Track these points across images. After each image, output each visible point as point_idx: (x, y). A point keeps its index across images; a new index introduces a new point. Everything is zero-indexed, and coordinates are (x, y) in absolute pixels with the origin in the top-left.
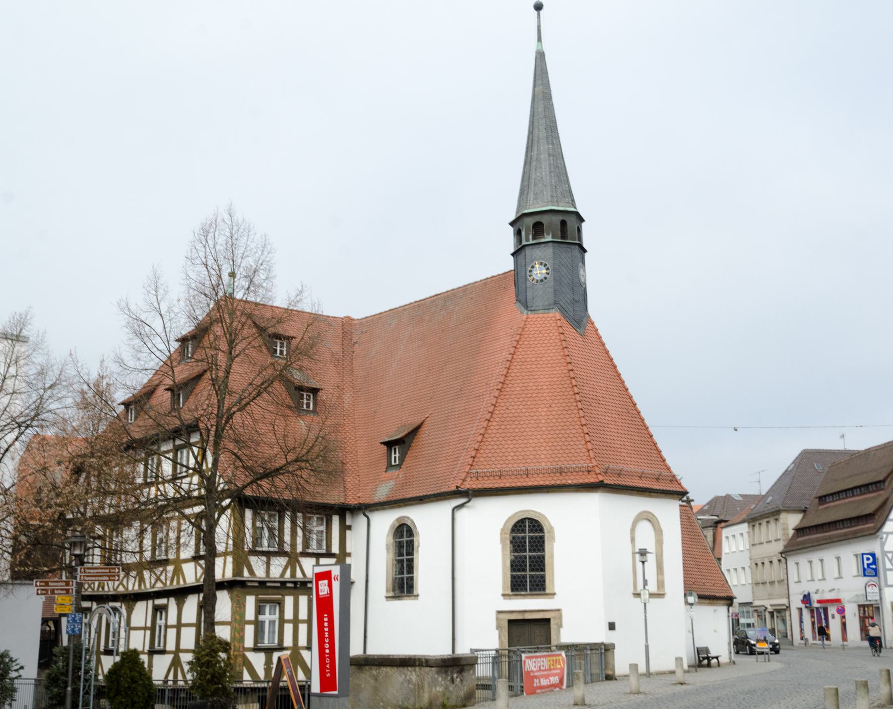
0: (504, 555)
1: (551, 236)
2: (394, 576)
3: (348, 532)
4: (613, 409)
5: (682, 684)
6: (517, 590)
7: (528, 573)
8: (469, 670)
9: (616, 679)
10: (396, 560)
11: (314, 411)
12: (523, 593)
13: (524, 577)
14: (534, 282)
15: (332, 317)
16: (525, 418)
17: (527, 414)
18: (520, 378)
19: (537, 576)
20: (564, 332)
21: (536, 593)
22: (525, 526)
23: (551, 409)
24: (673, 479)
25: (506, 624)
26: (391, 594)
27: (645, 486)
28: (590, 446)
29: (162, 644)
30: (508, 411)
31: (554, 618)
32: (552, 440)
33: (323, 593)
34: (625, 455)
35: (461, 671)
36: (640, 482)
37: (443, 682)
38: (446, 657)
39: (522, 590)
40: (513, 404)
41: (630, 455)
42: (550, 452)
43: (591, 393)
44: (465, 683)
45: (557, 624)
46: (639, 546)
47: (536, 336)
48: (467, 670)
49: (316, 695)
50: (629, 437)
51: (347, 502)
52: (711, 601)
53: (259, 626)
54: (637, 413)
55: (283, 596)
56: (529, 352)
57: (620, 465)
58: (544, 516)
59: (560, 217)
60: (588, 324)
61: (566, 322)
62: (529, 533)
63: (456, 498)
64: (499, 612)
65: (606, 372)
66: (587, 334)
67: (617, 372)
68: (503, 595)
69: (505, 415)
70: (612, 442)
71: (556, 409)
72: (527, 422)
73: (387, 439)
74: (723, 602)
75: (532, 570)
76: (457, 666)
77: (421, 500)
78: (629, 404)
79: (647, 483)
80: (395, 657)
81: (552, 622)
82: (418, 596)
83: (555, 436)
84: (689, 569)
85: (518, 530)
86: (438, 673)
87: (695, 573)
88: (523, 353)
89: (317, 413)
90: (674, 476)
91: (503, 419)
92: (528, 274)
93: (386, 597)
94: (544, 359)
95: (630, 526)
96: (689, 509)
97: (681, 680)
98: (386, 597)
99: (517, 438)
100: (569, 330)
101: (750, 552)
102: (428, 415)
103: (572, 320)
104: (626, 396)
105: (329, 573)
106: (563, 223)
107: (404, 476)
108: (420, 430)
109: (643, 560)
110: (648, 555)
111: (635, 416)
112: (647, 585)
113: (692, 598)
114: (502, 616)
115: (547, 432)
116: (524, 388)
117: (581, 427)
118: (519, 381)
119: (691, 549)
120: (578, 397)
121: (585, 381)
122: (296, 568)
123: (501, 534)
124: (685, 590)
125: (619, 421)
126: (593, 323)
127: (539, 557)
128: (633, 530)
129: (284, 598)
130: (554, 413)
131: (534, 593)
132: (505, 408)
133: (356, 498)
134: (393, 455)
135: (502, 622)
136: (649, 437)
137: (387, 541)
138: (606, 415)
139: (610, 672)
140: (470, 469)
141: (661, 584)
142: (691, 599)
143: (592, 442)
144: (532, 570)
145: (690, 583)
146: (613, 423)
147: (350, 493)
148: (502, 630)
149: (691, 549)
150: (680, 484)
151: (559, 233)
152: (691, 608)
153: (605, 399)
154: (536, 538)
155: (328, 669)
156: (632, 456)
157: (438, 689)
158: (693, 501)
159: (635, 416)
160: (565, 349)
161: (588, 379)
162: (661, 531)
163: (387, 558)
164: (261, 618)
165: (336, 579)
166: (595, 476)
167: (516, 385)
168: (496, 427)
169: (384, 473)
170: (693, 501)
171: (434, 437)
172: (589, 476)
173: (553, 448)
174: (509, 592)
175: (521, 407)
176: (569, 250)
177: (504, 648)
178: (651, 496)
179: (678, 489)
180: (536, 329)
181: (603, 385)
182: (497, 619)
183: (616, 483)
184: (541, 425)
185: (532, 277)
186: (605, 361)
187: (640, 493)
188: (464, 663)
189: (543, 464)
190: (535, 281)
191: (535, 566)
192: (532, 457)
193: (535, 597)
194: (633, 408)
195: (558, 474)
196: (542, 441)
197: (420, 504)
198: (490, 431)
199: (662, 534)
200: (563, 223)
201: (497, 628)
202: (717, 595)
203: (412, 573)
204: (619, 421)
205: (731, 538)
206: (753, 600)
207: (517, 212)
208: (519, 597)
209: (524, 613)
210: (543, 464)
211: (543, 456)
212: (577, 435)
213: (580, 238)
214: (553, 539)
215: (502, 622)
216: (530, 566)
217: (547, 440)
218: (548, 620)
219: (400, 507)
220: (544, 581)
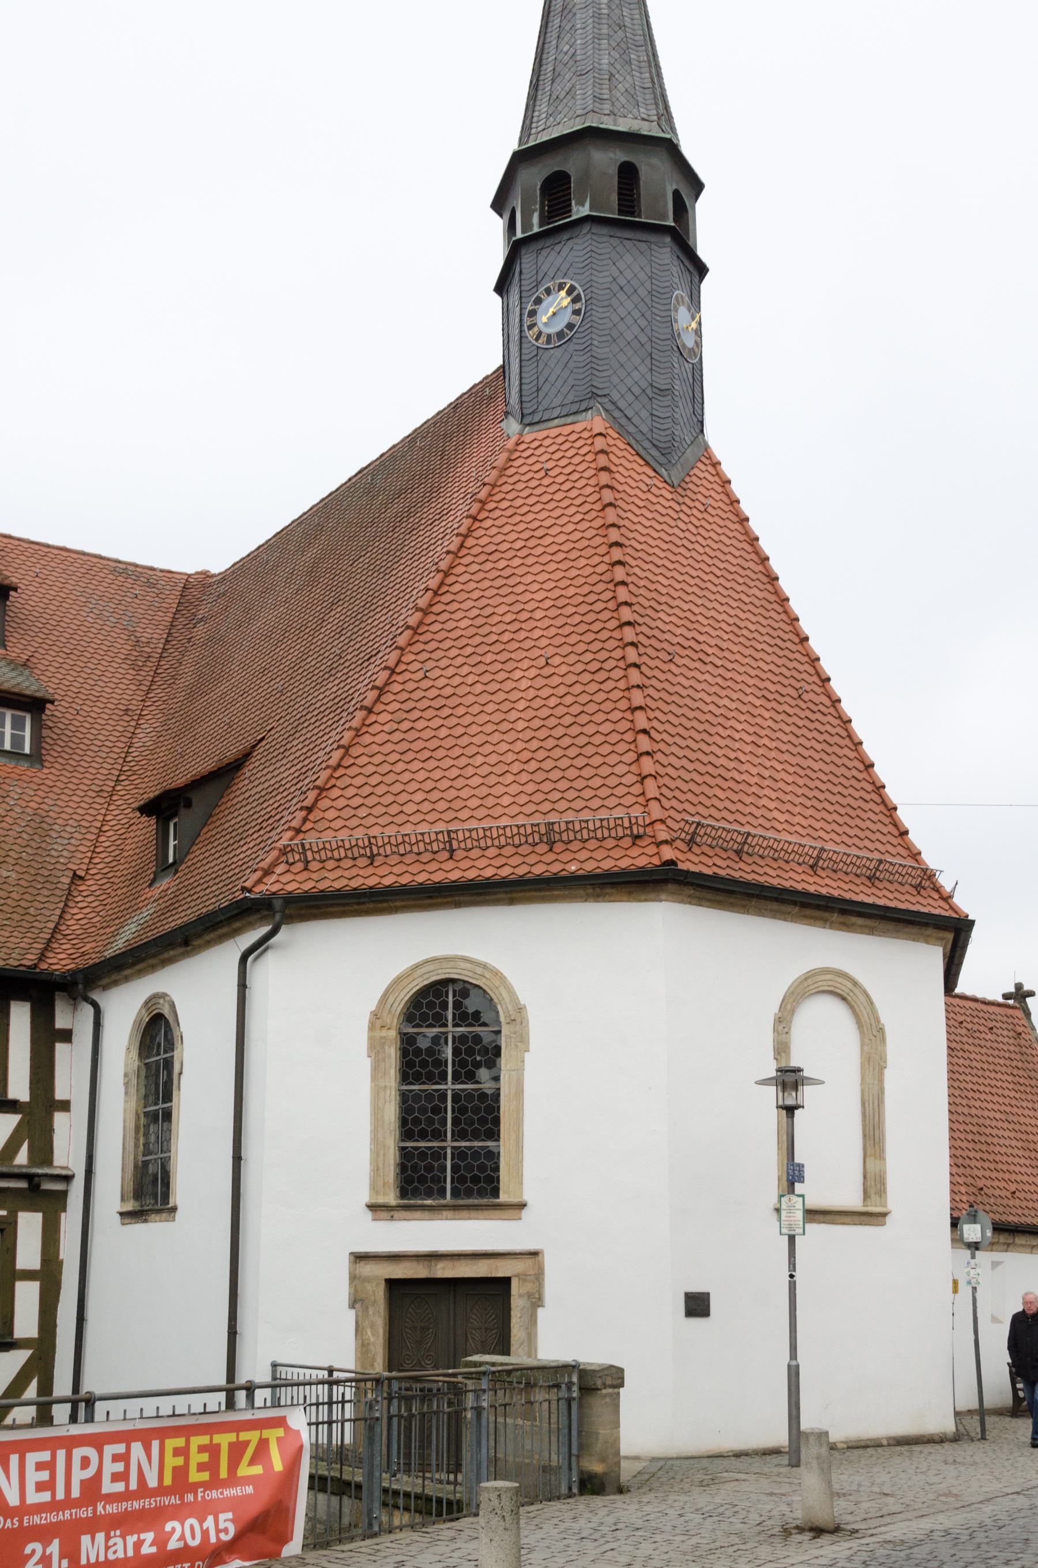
0: (377, 1093)
1: (587, 205)
2: (141, 1158)
3: (60, 1048)
5: (818, 1531)
6: (416, 1193)
7: (449, 1143)
9: (621, 1490)
10: (146, 1114)
11: (36, 757)
12: (429, 1202)
13: (438, 1155)
14: (541, 343)
15: (162, 571)
19: (476, 1154)
21: (470, 1201)
25: (379, 1293)
26: (130, 1206)
27: (824, 891)
28: (647, 765)
31: (522, 1277)
34: (772, 805)
39: (429, 1194)
45: (529, 1295)
50: (794, 760)
54: (828, 703)
58: (497, 973)
59: (618, 156)
60: (700, 465)
61: (622, 446)
62: (455, 1025)
64: (359, 1258)
66: (694, 479)
67: (777, 592)
68: (373, 1207)
70: (731, 765)
77: (186, 943)
81: (514, 1284)
82: (174, 1209)
84: (1005, 1158)
85: (424, 1018)
87: (1018, 1169)
89: (41, 762)
90: (929, 875)
92: (527, 322)
93: (122, 1214)
95: (773, 1008)
96: (1019, 1014)
97: (822, 1516)
98: (122, 1214)
103: (647, 444)
106: (628, 174)
108: (246, 772)
109: (790, 1102)
110: (808, 1092)
113: (978, 1227)
114: (368, 1269)
119: (1015, 1110)
120: (629, 634)
122: (21, 1145)
123: (372, 1027)
126: (716, 464)
127: (417, 1078)
128: (783, 1022)
131: (461, 1202)
135: (369, 1287)
136: (861, 767)
137: (126, 1065)
138: (723, 693)
139: (597, 1468)
148: (366, 1309)
149: (1015, 1110)
151: (615, 197)
152: (973, 1257)
158: (1031, 994)
159: (821, 707)
160: (610, 511)
162: (881, 1030)
163: (125, 1111)
166: (652, 850)
170: (1031, 994)
172: (635, 852)
174: (391, 1198)
176: (643, 246)
178: (848, 927)
182: (353, 1278)
184: (513, 715)
185: (536, 329)
187: (808, 912)
190: (543, 339)
193: (465, 1213)
195: (542, 848)
197: (186, 955)
198: (367, 739)
199: (883, 1040)
200: (628, 174)
201: (352, 1306)
208: (418, 1214)
214: (523, 1040)
215: (369, 1287)
216: (456, 1122)
218: (506, 1281)
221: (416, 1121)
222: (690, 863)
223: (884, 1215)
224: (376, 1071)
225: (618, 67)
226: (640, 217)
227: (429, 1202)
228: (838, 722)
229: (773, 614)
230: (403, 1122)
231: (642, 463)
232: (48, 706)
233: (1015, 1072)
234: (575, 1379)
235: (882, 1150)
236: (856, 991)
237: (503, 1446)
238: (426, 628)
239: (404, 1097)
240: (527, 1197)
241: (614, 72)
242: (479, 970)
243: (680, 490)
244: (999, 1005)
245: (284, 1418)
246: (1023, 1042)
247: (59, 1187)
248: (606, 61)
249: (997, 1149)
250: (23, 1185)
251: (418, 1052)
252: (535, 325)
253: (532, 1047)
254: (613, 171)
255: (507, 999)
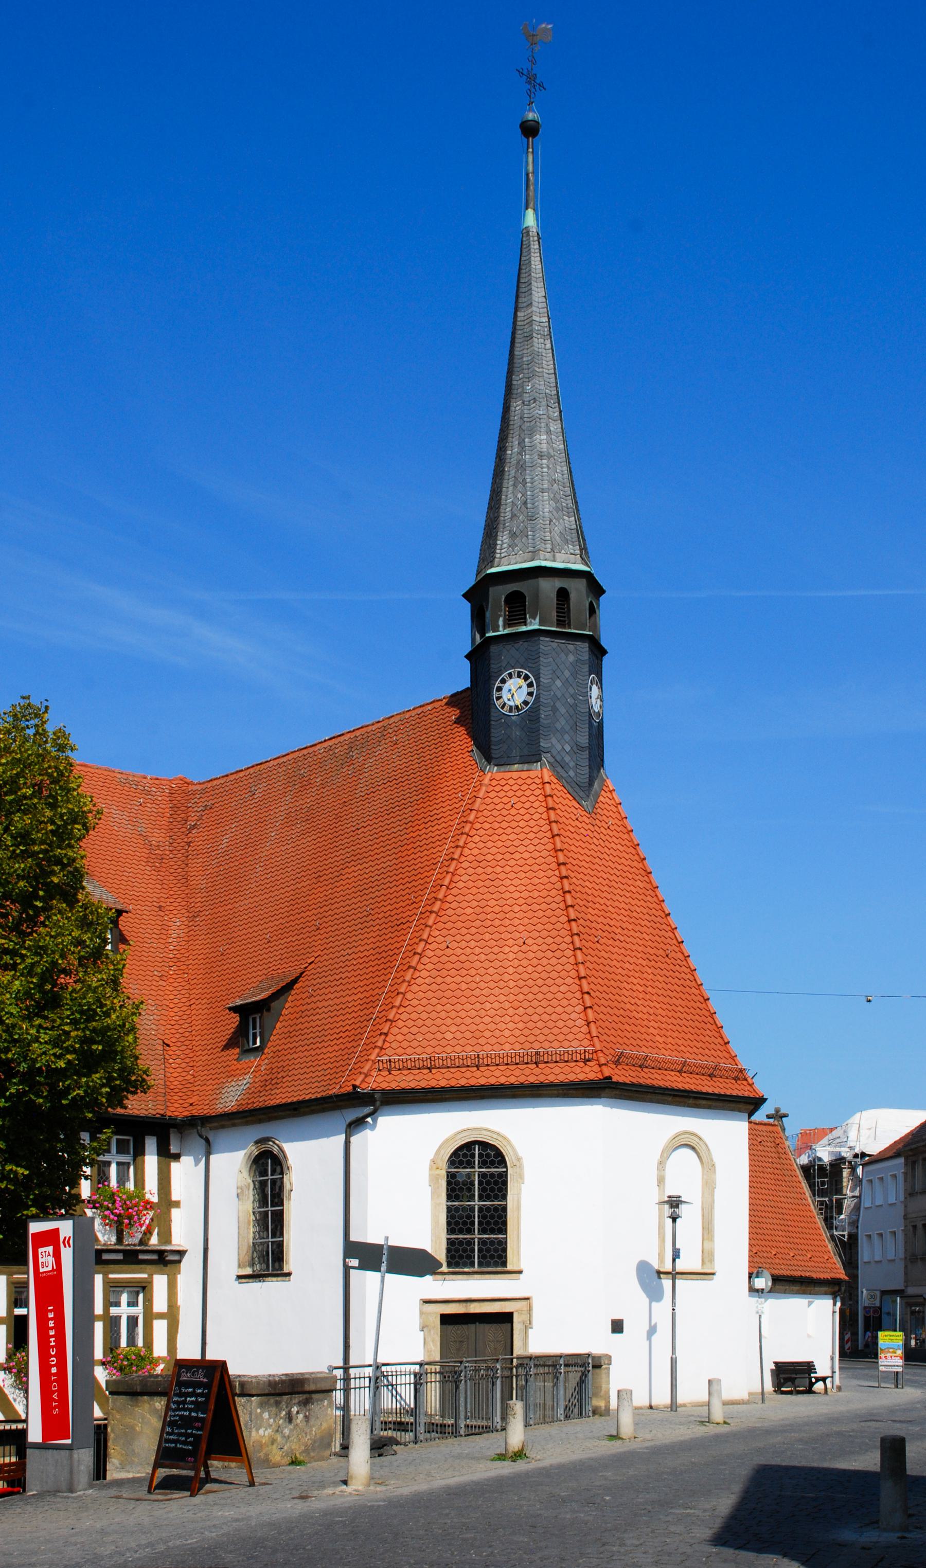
0: (435, 1206)
4: (640, 949)
6: (457, 1265)
7: (477, 1236)
8: (322, 1400)
12: (466, 1270)
13: (470, 1243)
16: (478, 964)
17: (483, 957)
18: (474, 891)
19: (492, 1242)
20: (556, 807)
21: (489, 1269)
22: (473, 1156)
23: (525, 948)
24: (740, 1075)
26: (248, 1271)
27: (687, 1087)
29: (140, 1343)
30: (449, 951)
32: (526, 1004)
33: (45, 1269)
35: (305, 1403)
36: (679, 1080)
37: (272, 1420)
38: (277, 1379)
39: (465, 1265)
40: (458, 938)
41: (664, 1032)
42: (521, 1026)
43: (599, 920)
44: (312, 1422)
46: (671, 1190)
47: (504, 812)
48: (318, 1400)
49: (36, 1446)
51: (169, 1114)
52: (803, 1288)
53: (112, 1324)
55: (151, 1276)
56: (490, 844)
57: (644, 1049)
59: (558, 583)
62: (479, 1168)
63: (354, 1106)
65: (630, 882)
66: (599, 810)
69: (444, 959)
71: (535, 948)
72: (482, 971)
73: (239, 1002)
74: (824, 1289)
75: (483, 1231)
76: (299, 1393)
77: (295, 1109)
78: (669, 940)
79: (691, 1081)
80: (307, 1376)
82: (289, 1274)
83: (531, 997)
85: (461, 1163)
86: (261, 1405)
88: (481, 845)
91: (440, 966)
94: (517, 856)
99: (463, 1000)
100: (564, 801)
101: (906, 1207)
102: (313, 959)
104: (664, 926)
105: (57, 1231)
106: (563, 595)
107: (268, 1067)
109: (675, 1216)
110: (683, 1207)
111: (679, 961)
112: (678, 1257)
115: (517, 990)
116: (478, 910)
117: (577, 981)
118: (471, 897)
121: (590, 898)
123: (431, 1169)
124: (750, 1266)
125: (649, 971)
127: (496, 1209)
128: (662, 1164)
129: (152, 1278)
130: (531, 955)
132: (444, 946)
133: (186, 1105)
134: (251, 1032)
140: (378, 1056)
141: (707, 1256)
142: (761, 1283)
143: (596, 1007)
144: (483, 1231)
145: (769, 1255)
146: (637, 975)
147: (176, 1098)
150: (751, 1085)
153: (626, 932)
154: (492, 1175)
155: (55, 1401)
156: (668, 1034)
157: (261, 1432)
158: (786, 1116)
159: (679, 961)
161: (596, 893)
164: (114, 1311)
165: (66, 1242)
166: (597, 1068)
167: (464, 904)
168: (427, 981)
169: (235, 1063)
170: (786, 1116)
171: (321, 998)
172: (587, 1069)
173: (526, 1018)
175: (473, 944)
177: (432, 1359)
179: (746, 1094)
180: (505, 800)
181: (623, 905)
182: (421, 1313)
183: (634, 1081)
184: (506, 977)
185: (501, 700)
186: (629, 862)
188: (312, 1387)
189: (507, 1046)
191: (488, 1223)
192: (487, 1034)
193: (487, 1276)
194: (677, 949)
196: (507, 1005)
197: (294, 1116)
198: (415, 988)
200: (563, 595)
202: (814, 1276)
203: (282, 1235)
204: (649, 971)
205: (877, 1183)
206: (906, 1287)
207: (478, 573)
209: (469, 1304)
210: (507, 1046)
211: (507, 1033)
212: (569, 995)
213: (595, 627)
214: (521, 1176)
217: (516, 1004)
219: (260, 1121)
220: (505, 1250)
221: (457, 1223)
222: (620, 1075)
223: (713, 1274)
224: (434, 1194)
225: (555, 513)
226: (570, 628)
227: (466, 1270)
228: (688, 970)
229: (649, 898)
230: (449, 1223)
231: (571, 798)
232: (124, 914)
233: (776, 1171)
234: (590, 1361)
235: (713, 1236)
236: (701, 1143)
237: (181, 1495)
238: (444, 912)
239: (449, 1209)
240: (523, 1266)
241: (552, 518)
242: (495, 1136)
243: (593, 815)
244: (765, 1124)
245: (865, 1308)
246: (780, 1150)
247: (176, 1258)
248: (546, 510)
249: (765, 1226)
250: (155, 1257)
251: (457, 1183)
252: (501, 697)
253: (525, 1181)
254: (554, 595)
255: (512, 1153)
